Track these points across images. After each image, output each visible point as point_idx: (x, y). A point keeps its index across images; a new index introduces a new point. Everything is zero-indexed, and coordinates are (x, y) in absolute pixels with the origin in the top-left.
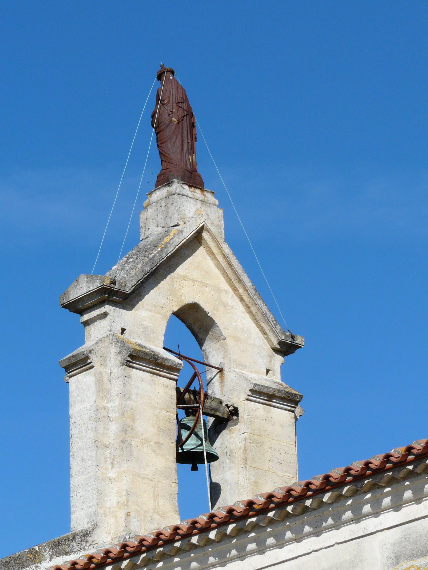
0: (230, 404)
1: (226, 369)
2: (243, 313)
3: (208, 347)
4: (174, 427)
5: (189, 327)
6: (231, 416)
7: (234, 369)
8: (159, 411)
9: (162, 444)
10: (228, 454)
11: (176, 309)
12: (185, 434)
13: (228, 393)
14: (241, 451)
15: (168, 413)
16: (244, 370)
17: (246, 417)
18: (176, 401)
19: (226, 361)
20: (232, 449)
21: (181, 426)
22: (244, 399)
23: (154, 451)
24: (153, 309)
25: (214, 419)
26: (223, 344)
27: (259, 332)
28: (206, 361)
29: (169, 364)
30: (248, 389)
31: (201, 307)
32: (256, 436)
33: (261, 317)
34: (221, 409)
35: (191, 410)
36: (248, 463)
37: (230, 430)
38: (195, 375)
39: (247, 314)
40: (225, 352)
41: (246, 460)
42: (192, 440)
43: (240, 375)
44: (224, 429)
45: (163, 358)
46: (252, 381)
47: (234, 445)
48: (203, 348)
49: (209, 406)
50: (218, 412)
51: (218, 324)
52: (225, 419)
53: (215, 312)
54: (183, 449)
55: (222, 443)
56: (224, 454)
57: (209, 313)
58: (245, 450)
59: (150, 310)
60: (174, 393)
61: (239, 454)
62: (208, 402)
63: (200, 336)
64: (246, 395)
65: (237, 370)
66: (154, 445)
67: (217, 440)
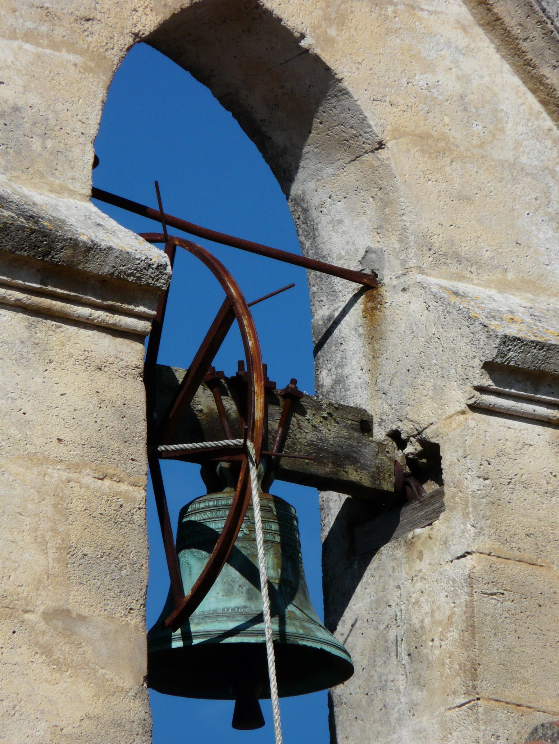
0: (406, 429)
1: (388, 277)
2: (464, 29)
3: (312, 185)
4: (138, 542)
5: (229, 101)
6: (413, 483)
7: (420, 278)
8: (65, 475)
9: (82, 618)
10: (403, 648)
11: (149, 23)
12: (194, 564)
13: (397, 383)
14: (454, 634)
15: (107, 482)
16: (470, 281)
17: (473, 485)
18: (142, 427)
19: (390, 243)
20: (418, 626)
21: (179, 535)
22: (464, 407)
23: (47, 651)
24: (44, 28)
25: (345, 497)
26: (374, 169)
27: (538, 107)
28: (308, 244)
29: (106, 270)
30: (478, 363)
31: (268, 13)
32: (523, 566)
33: (540, 43)
34: (368, 453)
35: (225, 465)
36: (485, 687)
37: (410, 544)
38: (228, 315)
39: (479, 31)
40: (385, 203)
41: (472, 670)
42: (229, 592)
43: (448, 305)
44: (386, 539)
45: (74, 244)
46: (493, 324)
47: (426, 608)
48: (296, 189)
49: (311, 444)
50: (350, 469)
51: (345, 84)
52: (392, 493)
53: (332, 32)
54: (187, 636)
55: (378, 602)
56: (387, 650)
57: (303, 36)
58: (471, 627)
59: (29, 36)
60: (136, 393)
61: (446, 645)
62: (305, 424)
63: (279, 138)
64: (469, 388)
65: (435, 281)
66: (43, 625)
67: (359, 589)
